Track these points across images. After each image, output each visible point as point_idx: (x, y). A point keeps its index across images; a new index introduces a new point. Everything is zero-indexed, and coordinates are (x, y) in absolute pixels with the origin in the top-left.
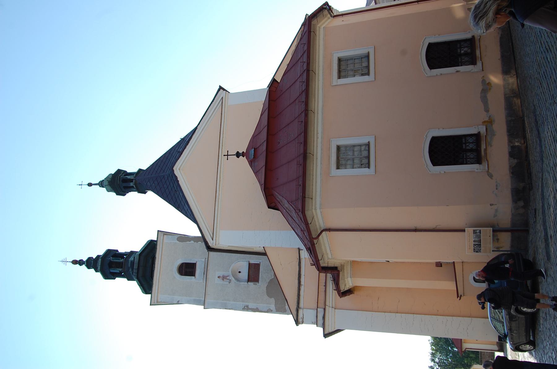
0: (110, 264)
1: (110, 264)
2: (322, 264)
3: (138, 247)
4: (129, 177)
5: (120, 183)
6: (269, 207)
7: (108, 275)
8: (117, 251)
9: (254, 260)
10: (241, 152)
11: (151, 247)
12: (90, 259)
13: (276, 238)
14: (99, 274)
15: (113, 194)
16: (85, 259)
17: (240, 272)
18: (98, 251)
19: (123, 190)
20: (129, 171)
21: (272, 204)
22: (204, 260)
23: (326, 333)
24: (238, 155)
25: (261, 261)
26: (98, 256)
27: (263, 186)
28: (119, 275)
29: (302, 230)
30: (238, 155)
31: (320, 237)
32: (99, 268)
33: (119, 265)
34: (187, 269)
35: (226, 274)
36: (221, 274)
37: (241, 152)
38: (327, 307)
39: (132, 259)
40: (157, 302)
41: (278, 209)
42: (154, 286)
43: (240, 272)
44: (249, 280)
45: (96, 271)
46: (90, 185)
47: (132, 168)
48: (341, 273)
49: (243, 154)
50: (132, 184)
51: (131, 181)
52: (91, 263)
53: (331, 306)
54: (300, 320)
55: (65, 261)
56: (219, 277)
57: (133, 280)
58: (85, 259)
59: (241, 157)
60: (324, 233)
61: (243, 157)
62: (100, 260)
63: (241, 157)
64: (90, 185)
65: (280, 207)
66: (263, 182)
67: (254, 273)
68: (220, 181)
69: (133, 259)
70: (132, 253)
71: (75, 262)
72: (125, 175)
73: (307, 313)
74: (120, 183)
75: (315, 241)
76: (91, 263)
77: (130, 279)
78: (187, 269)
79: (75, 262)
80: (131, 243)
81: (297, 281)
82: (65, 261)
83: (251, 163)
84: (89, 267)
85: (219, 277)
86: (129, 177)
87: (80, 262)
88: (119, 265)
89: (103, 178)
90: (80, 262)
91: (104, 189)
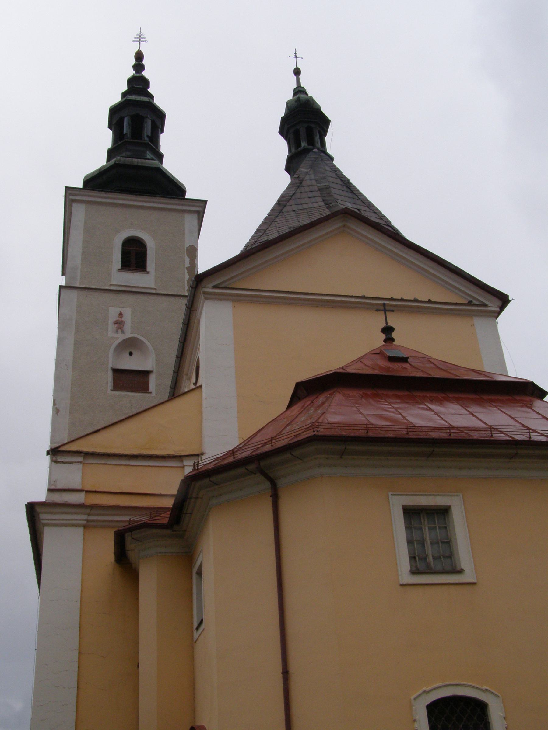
0: (136, 118)
1: (136, 118)
2: (128, 538)
3: (171, 165)
4: (317, 138)
5: (304, 124)
6: (299, 386)
7: (117, 116)
8: (162, 131)
9: (158, 385)
10: (394, 335)
11: (170, 189)
12: (146, 83)
13: (223, 416)
14: (118, 99)
15: (281, 112)
16: (145, 73)
17: (131, 354)
18: (161, 95)
19: (292, 131)
20: (327, 139)
21: (307, 390)
22: (153, 286)
23: (38, 509)
24: (388, 330)
25: (154, 394)
26: (152, 97)
27: (341, 371)
28: (118, 137)
29: (272, 439)
30: (388, 330)
31: (262, 478)
32: (131, 97)
33: (137, 131)
34: (134, 256)
35: (128, 326)
36: (128, 318)
37: (394, 335)
38: (88, 511)
39: (149, 155)
40: (73, 201)
41: (290, 405)
42: (103, 194)
43: (131, 354)
44: (116, 371)
45: (124, 94)
46: (297, 72)
47: (334, 142)
48: (168, 532)
49: (389, 340)
50: (304, 144)
51: (311, 142)
52: (138, 84)
53: (91, 518)
54: (59, 459)
55: (140, 39)
56: (121, 314)
57: (109, 158)
58: (145, 73)
59: (384, 336)
60: (268, 484)
61: (385, 341)
62: (146, 99)
63: (384, 336)
64: (297, 72)
65: (296, 408)
66: (351, 370)
67: (131, 380)
68: (328, 295)
69: (149, 157)
70: (160, 157)
71: (139, 56)
72: (320, 133)
73: (73, 475)
74: (304, 124)
75: (251, 467)
76: (138, 84)
77: (111, 153)
78: (134, 256)
79: (139, 56)
80: (177, 154)
81: (135, 452)
82: (140, 39)
83: (380, 353)
84: (131, 81)
85: (121, 314)
86: (317, 138)
87: (139, 66)
88: (137, 131)
89: (311, 92)
90: (139, 66)
91: (290, 96)
